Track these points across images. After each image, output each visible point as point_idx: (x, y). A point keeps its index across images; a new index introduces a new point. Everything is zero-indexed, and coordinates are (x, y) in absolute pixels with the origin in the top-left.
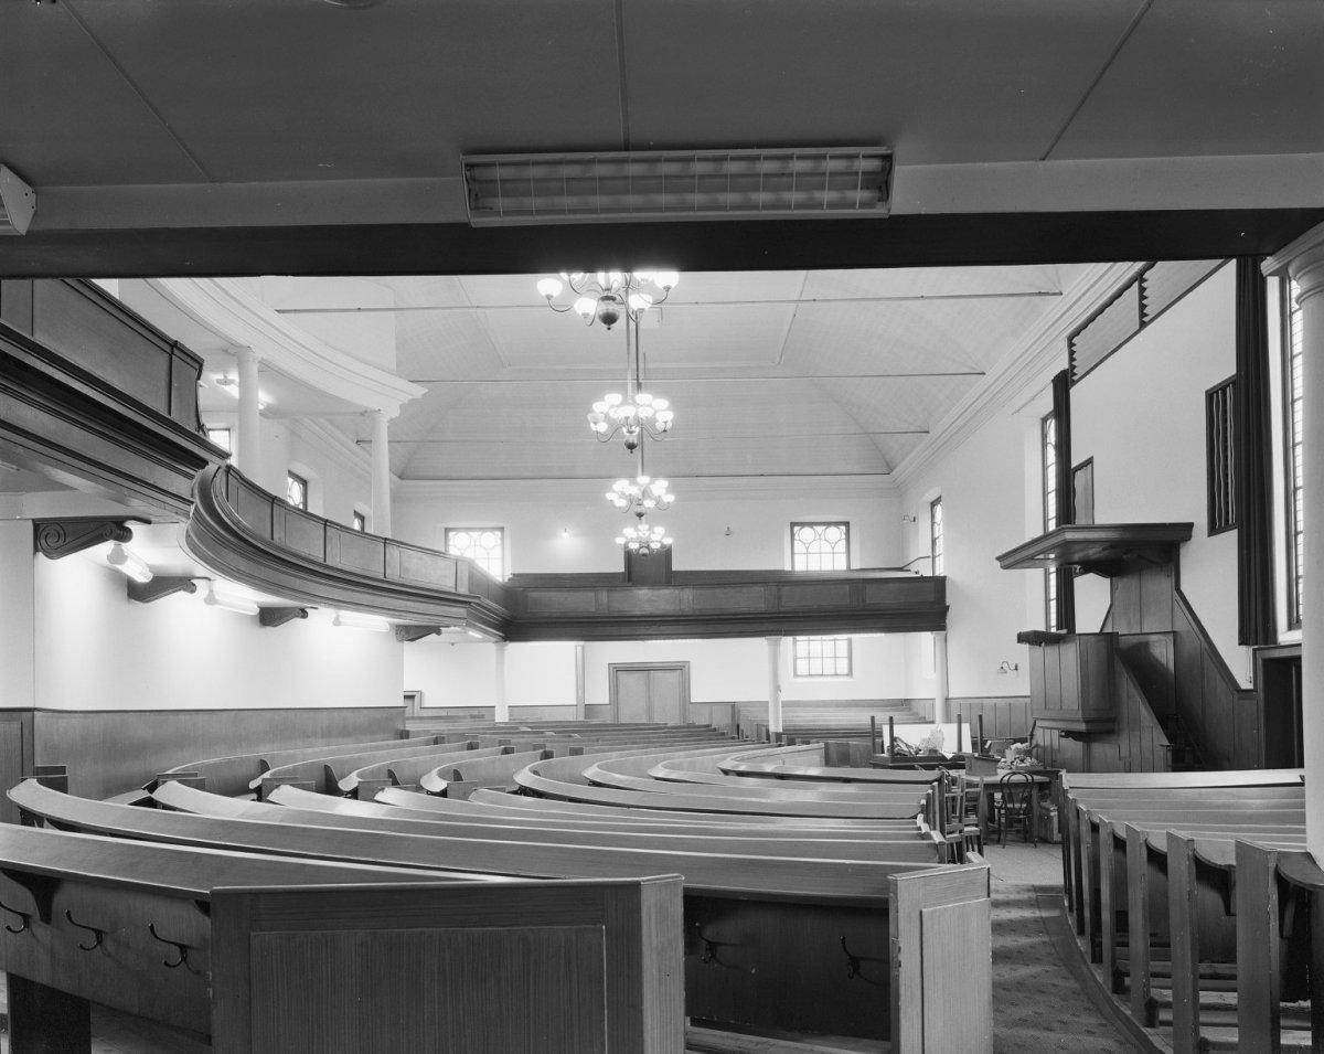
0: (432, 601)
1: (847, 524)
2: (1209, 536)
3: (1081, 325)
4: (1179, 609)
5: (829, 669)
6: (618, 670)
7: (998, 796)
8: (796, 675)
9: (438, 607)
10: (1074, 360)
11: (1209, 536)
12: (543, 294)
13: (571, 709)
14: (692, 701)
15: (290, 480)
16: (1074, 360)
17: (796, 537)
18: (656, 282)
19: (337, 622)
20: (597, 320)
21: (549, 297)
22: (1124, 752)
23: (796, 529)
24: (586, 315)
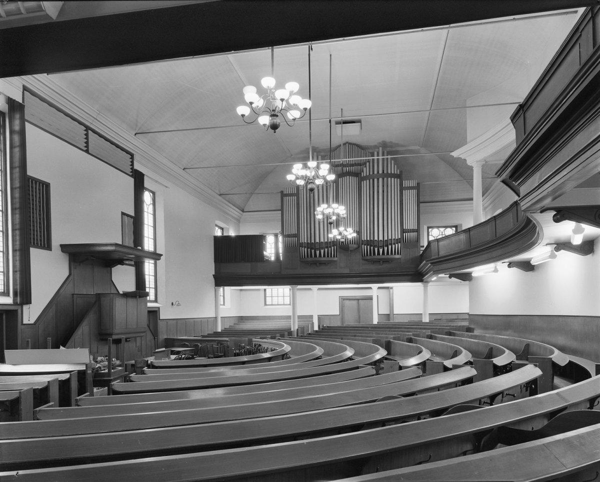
0: (444, 262)
1: (428, 228)
2: (51, 250)
3: (80, 121)
4: (113, 287)
5: (281, 302)
6: (343, 299)
7: (99, 359)
8: (266, 304)
9: (322, 272)
10: (86, 143)
11: (51, 250)
12: (240, 114)
13: (213, 319)
14: (161, 318)
15: (217, 228)
16: (86, 143)
17: (430, 234)
18: (301, 98)
19: (496, 270)
20: (269, 128)
21: (243, 116)
22: (138, 344)
23: (430, 230)
24: (264, 125)
